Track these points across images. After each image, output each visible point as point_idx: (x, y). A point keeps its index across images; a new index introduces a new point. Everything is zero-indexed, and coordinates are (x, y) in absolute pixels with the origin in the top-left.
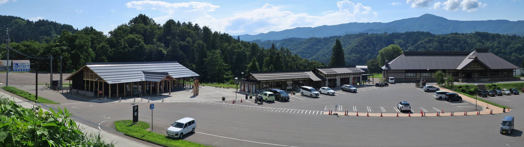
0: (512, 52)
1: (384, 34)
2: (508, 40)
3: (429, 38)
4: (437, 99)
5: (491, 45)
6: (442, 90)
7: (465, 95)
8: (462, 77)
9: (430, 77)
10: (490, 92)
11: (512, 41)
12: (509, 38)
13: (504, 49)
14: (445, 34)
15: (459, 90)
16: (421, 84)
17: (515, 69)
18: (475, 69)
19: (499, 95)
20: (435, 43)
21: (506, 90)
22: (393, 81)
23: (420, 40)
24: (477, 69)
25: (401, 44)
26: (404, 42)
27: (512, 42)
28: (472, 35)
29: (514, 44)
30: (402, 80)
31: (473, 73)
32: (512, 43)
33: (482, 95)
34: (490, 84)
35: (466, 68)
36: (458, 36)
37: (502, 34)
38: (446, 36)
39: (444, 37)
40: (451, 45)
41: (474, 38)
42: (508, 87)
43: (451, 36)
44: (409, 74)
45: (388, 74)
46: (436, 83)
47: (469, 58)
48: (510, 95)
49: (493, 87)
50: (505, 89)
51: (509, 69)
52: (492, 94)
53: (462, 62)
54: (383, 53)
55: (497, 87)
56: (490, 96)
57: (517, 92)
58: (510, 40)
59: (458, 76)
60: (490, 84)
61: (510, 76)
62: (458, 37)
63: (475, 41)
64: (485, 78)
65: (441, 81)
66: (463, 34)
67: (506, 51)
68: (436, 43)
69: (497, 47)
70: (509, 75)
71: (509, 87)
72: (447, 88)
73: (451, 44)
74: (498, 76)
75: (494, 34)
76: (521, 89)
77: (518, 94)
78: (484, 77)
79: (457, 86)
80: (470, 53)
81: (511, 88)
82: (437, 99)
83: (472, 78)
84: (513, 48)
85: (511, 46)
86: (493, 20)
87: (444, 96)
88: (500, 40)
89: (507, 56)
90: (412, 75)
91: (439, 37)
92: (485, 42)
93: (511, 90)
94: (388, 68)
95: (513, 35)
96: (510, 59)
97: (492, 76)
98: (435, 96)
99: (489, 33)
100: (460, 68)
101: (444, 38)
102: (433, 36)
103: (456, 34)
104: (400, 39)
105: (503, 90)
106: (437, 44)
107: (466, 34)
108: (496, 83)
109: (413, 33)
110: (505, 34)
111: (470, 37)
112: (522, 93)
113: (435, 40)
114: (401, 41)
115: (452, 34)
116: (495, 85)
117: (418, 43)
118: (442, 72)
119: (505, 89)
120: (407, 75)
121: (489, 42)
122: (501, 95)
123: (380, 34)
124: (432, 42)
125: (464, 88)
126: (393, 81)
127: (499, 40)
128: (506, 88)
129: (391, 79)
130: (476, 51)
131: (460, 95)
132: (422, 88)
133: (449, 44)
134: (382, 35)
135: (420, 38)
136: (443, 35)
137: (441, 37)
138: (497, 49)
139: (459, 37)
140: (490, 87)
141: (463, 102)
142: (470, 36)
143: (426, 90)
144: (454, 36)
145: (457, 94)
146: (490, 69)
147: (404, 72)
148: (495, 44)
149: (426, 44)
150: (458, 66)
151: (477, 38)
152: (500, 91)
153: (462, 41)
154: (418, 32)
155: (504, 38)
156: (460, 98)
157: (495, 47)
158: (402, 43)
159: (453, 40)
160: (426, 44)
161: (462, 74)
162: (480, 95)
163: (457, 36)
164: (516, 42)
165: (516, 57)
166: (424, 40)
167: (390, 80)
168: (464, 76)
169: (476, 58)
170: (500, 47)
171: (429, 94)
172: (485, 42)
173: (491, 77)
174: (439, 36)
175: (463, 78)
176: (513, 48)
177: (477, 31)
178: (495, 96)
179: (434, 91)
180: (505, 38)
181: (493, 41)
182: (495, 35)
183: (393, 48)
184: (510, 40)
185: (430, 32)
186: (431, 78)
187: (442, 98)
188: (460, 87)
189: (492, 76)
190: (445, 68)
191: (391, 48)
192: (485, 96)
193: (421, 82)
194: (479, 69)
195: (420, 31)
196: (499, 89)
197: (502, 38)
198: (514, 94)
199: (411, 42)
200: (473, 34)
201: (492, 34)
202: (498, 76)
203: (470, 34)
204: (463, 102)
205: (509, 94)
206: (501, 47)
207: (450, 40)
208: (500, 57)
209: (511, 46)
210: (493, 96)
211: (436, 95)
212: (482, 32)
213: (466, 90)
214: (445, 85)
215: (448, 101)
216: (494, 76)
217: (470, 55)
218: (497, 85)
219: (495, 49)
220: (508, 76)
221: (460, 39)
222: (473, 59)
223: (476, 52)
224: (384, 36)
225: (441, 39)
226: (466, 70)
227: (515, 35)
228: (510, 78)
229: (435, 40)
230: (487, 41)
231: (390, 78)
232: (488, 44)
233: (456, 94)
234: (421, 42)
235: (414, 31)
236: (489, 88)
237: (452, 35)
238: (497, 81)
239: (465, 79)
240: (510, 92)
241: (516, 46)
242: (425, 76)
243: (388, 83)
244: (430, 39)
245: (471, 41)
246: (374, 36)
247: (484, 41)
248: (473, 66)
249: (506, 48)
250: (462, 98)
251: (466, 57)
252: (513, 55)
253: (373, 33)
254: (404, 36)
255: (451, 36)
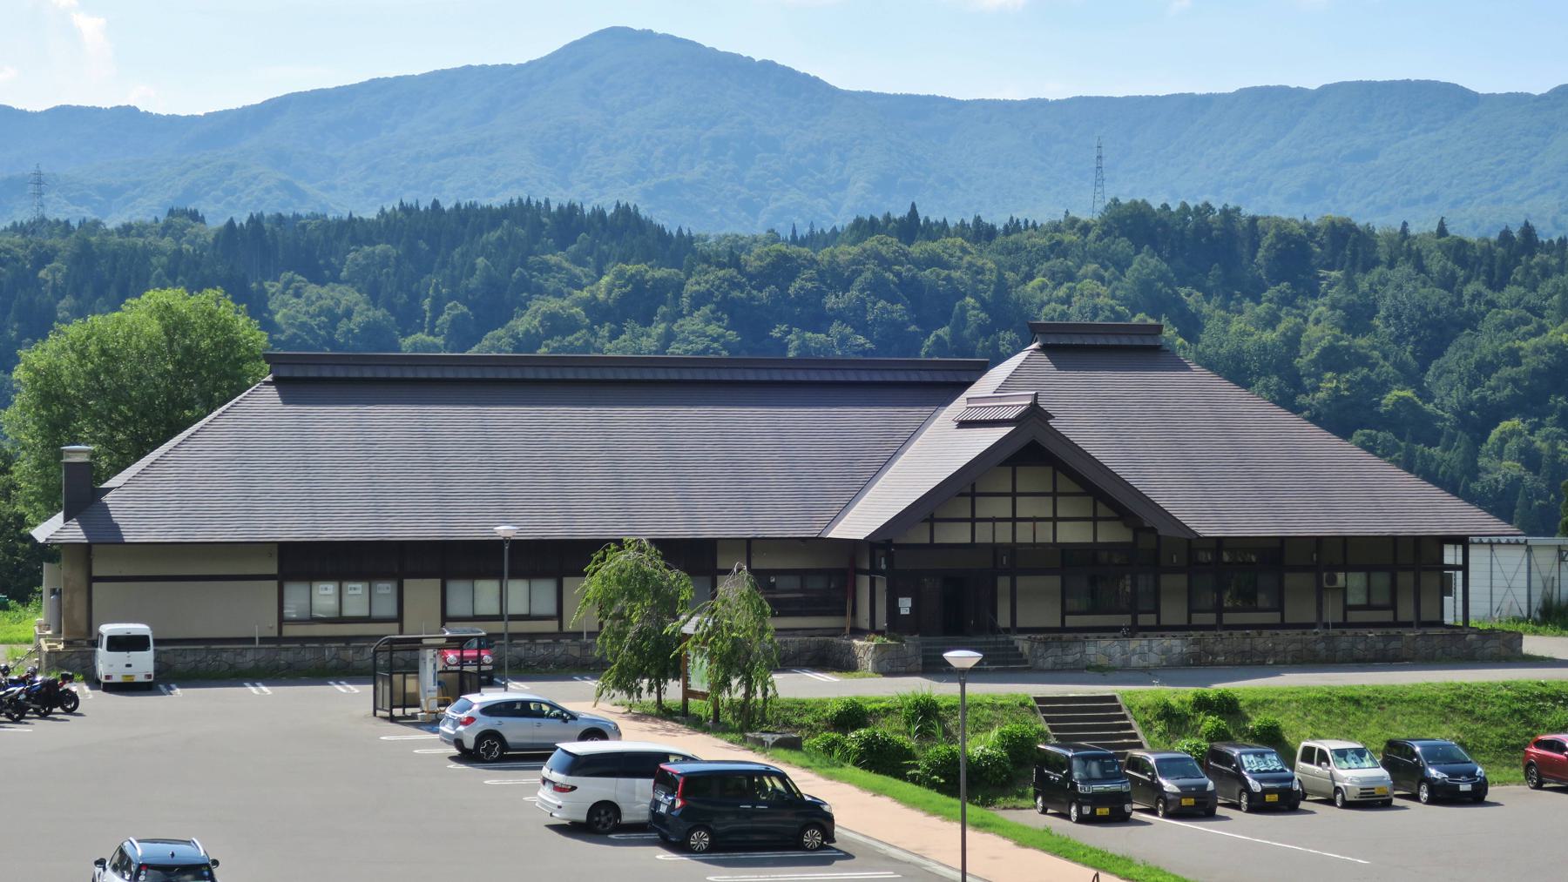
0: (1495, 414)
1: (166, 229)
2: (1448, 283)
3: (631, 269)
4: (571, 829)
5: (1269, 336)
6: (637, 738)
7: (878, 792)
8: (882, 623)
9: (552, 626)
10: (1168, 767)
11: (1490, 294)
12: (1462, 261)
13: (1412, 378)
14: (804, 231)
15: (834, 743)
16: (426, 683)
17: (1462, 541)
18: (1024, 534)
19: (1258, 805)
20: (692, 324)
21: (1341, 754)
22: (142, 664)
23: (540, 290)
24: (1044, 534)
25: (343, 326)
26: (379, 313)
27: (1491, 304)
28: (1070, 237)
29: (1509, 326)
30: (249, 659)
31: (1003, 583)
32: (1493, 319)
33: (1081, 800)
34: (1180, 694)
35: (932, 520)
36: (931, 246)
37: (1383, 223)
38: (806, 251)
39: (783, 258)
40: (861, 340)
41: (1092, 267)
42: (1373, 729)
43: (855, 250)
44: (325, 596)
45: (96, 586)
46: (592, 685)
47: (964, 424)
48: (1385, 804)
49: (1209, 722)
50: (1328, 745)
51: (1394, 540)
52: (1185, 792)
53: (889, 462)
54: (66, 379)
55: (1255, 722)
56: (1167, 815)
57: (1471, 774)
58: (1469, 289)
59: (843, 613)
60: (1180, 694)
61: (1406, 612)
62: (933, 261)
63: (1100, 301)
64: (1135, 630)
65: (647, 646)
66: (982, 233)
67: (1427, 396)
68: (708, 322)
69: (1333, 359)
70: (1393, 606)
71: (1384, 726)
72: (706, 730)
73: (862, 328)
74: (1273, 618)
75: (1306, 227)
76: (1514, 748)
77: (1477, 797)
78: (1125, 620)
79: (822, 703)
80: (983, 368)
81: (1399, 733)
82: (571, 829)
83: (994, 630)
84: (1507, 372)
85: (1486, 343)
86: (1300, 91)
87: (636, 796)
88: (1364, 286)
89: (1436, 451)
90: (356, 597)
91: (735, 262)
92: (1209, 308)
93: (1398, 758)
94: (86, 532)
95: (1506, 236)
96: (1475, 478)
97: (1210, 618)
98: (546, 794)
99: (1248, 211)
100: (858, 524)
101: (782, 268)
102: (678, 249)
103: (910, 228)
104: (336, 279)
105: (1308, 755)
106: (713, 329)
107: (1007, 231)
108: (1244, 687)
109: (471, 220)
110: (1422, 224)
111: (1056, 263)
112: (1525, 789)
113: (691, 287)
114: (349, 296)
115: (865, 228)
116: (1227, 707)
117: (524, 323)
118: (653, 565)
119: (1328, 745)
120: (297, 598)
121: (1247, 304)
122: (1285, 800)
123: (126, 230)
124: (662, 309)
125: (886, 730)
126: (142, 664)
127: (1351, 286)
128: (1348, 735)
129: (117, 644)
130: (1045, 349)
131: (810, 783)
132: (433, 723)
133: (835, 328)
134: (140, 242)
135: (546, 268)
136: (774, 237)
137: (752, 262)
138: (1329, 382)
139: (945, 265)
140: (1173, 719)
141: (848, 856)
142: (1058, 249)
143: (469, 743)
144: (884, 250)
145: (782, 777)
146: (1193, 544)
147: (272, 568)
148: (1312, 331)
149: (605, 332)
150: (847, 506)
151: (1122, 265)
152: (1273, 762)
153: (970, 300)
154: (521, 213)
155: (1404, 269)
156: (817, 817)
157: (1314, 362)
158: (357, 319)
159: (878, 288)
160: (605, 332)
161: (881, 586)
162: (1058, 796)
163: (916, 250)
164: (1532, 298)
165: (1530, 459)
166: (585, 294)
167: (102, 651)
168: (905, 605)
169: (1035, 415)
170: (1363, 360)
171: (495, 780)
172: (1206, 309)
173: (1198, 619)
174: (732, 255)
175: (897, 626)
176: (1507, 372)
177: (1124, 200)
178: (1220, 811)
179: (535, 755)
180: (1420, 268)
181: (1287, 301)
182: (1312, 232)
183: (176, 326)
184: (1469, 289)
185: (643, 212)
186: (561, 634)
187: (625, 819)
188: (852, 716)
189: (1210, 618)
190: (707, 530)
191: (154, 327)
192: (1103, 811)
193: (430, 665)
194: (1072, 534)
195: (538, 197)
196: (1271, 738)
197: (1391, 265)
198: (1431, 801)
199: (444, 318)
200: (1086, 229)
201: (1279, 224)
202: (1273, 618)
203: (1056, 228)
204: (848, 856)
205: (1370, 801)
206: (1376, 354)
207: (846, 290)
208: (1369, 447)
209: (1486, 343)
210: (1199, 808)
211: (559, 789)
212: (1174, 207)
213: (909, 754)
214: (688, 693)
215: (681, 846)
216: (1229, 618)
217: (977, 390)
218: (1254, 705)
219: (1307, 382)
220: (1387, 616)
221: (948, 279)
222: (1005, 431)
223: (1043, 357)
224: (167, 243)
225: (751, 277)
226: (932, 546)
227: (1528, 231)
228: (1409, 633)
229: (691, 287)
230: (1229, 296)
231: (107, 629)
232: (1234, 327)
233: (770, 773)
234: (552, 317)
235: (485, 202)
236: (1160, 727)
237: (871, 243)
238: (1262, 663)
239: (911, 645)
240: (1382, 772)
241: (1537, 351)
242: (494, 609)
243: (78, 688)
244: (638, 282)
245: (1067, 301)
246: (59, 243)
247: (1191, 298)
248: (1002, 508)
249: (1424, 369)
250: (829, 818)
251: (929, 419)
252: (1503, 440)
253: (51, 216)
254: (380, 248)
255: (855, 250)
